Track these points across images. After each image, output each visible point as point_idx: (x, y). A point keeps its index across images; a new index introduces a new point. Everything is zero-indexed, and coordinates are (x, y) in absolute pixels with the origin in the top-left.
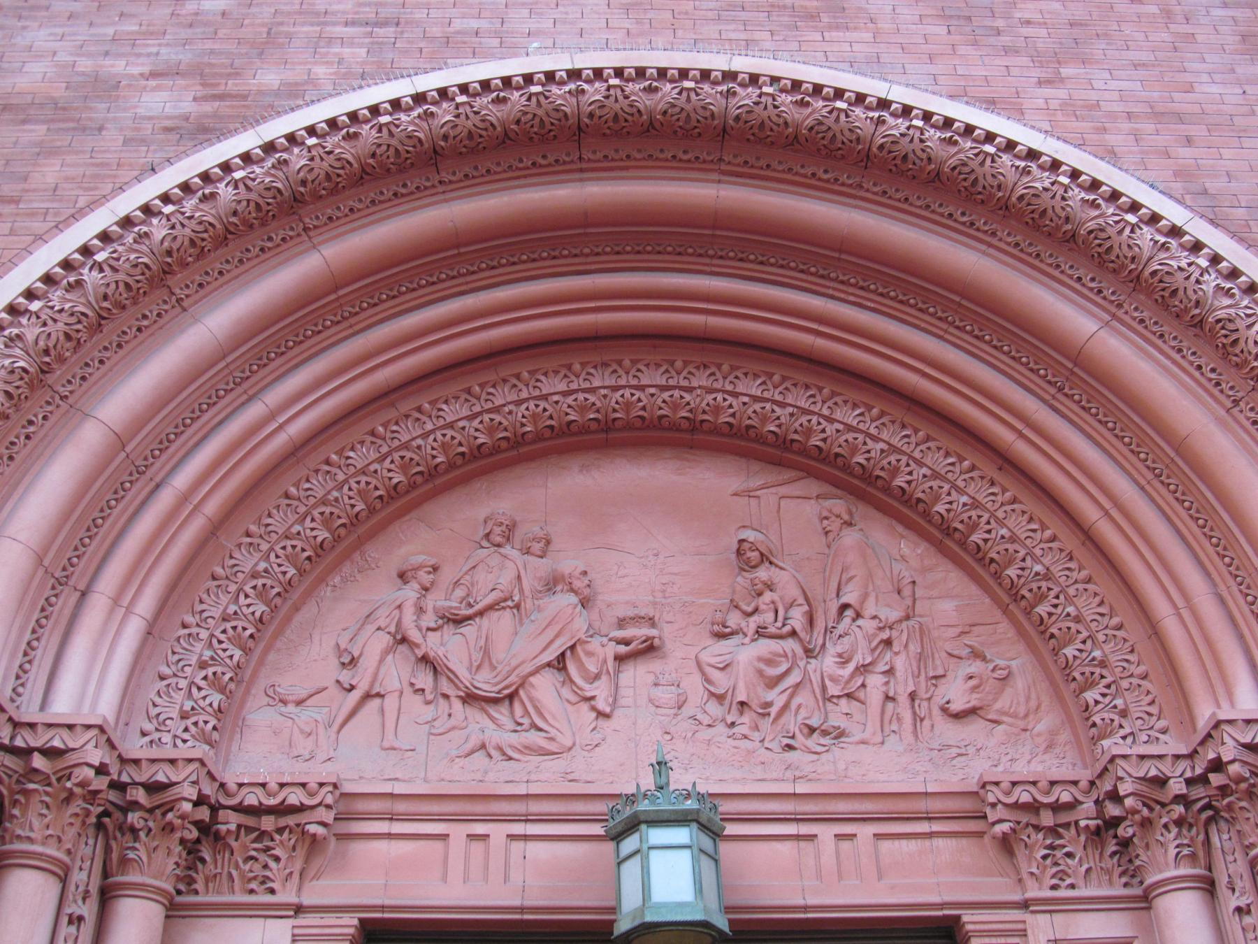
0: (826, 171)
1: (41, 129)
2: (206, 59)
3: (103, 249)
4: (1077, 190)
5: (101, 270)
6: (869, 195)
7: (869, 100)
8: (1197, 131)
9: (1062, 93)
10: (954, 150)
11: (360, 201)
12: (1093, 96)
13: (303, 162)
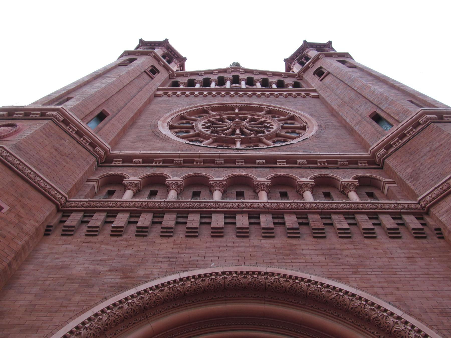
0: (295, 300)
1: (77, 285)
2: (124, 267)
3: (88, 323)
4: (368, 306)
5: (87, 330)
6: (308, 307)
7: (305, 280)
8: (400, 286)
9: (359, 276)
10: (331, 294)
11: (163, 309)
12: (368, 276)
13: (148, 298)
